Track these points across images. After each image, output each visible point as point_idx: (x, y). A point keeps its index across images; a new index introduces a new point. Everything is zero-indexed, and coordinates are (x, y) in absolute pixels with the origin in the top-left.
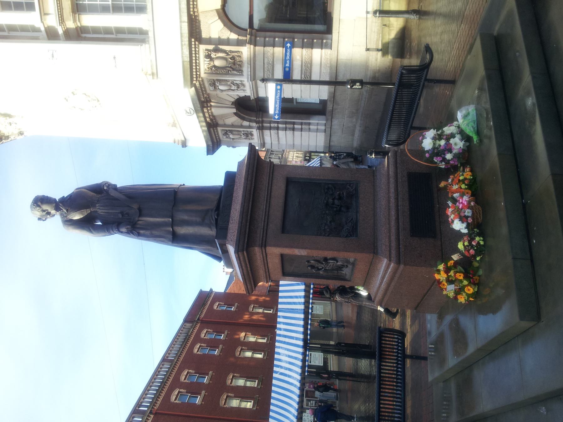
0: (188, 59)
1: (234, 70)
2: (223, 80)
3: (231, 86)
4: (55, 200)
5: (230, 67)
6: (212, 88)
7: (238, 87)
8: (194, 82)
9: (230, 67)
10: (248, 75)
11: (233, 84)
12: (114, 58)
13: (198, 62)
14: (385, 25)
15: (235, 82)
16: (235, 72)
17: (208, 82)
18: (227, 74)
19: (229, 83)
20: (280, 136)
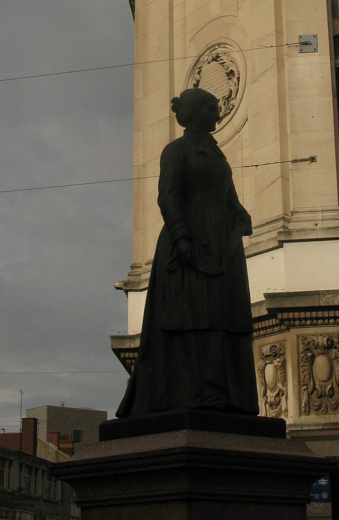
0: (322, 304)
1: (309, 395)
2: (285, 373)
3: (272, 390)
4: (185, 131)
5: (314, 388)
6: (266, 350)
7: (271, 405)
8: (279, 316)
9: (314, 388)
10: (302, 425)
11: (278, 395)
12: (313, 159)
13: (320, 321)
14: (306, 44)
15: (283, 398)
16: (304, 399)
17: (279, 342)
18: (300, 383)
19: (280, 385)
20: (272, 233)
